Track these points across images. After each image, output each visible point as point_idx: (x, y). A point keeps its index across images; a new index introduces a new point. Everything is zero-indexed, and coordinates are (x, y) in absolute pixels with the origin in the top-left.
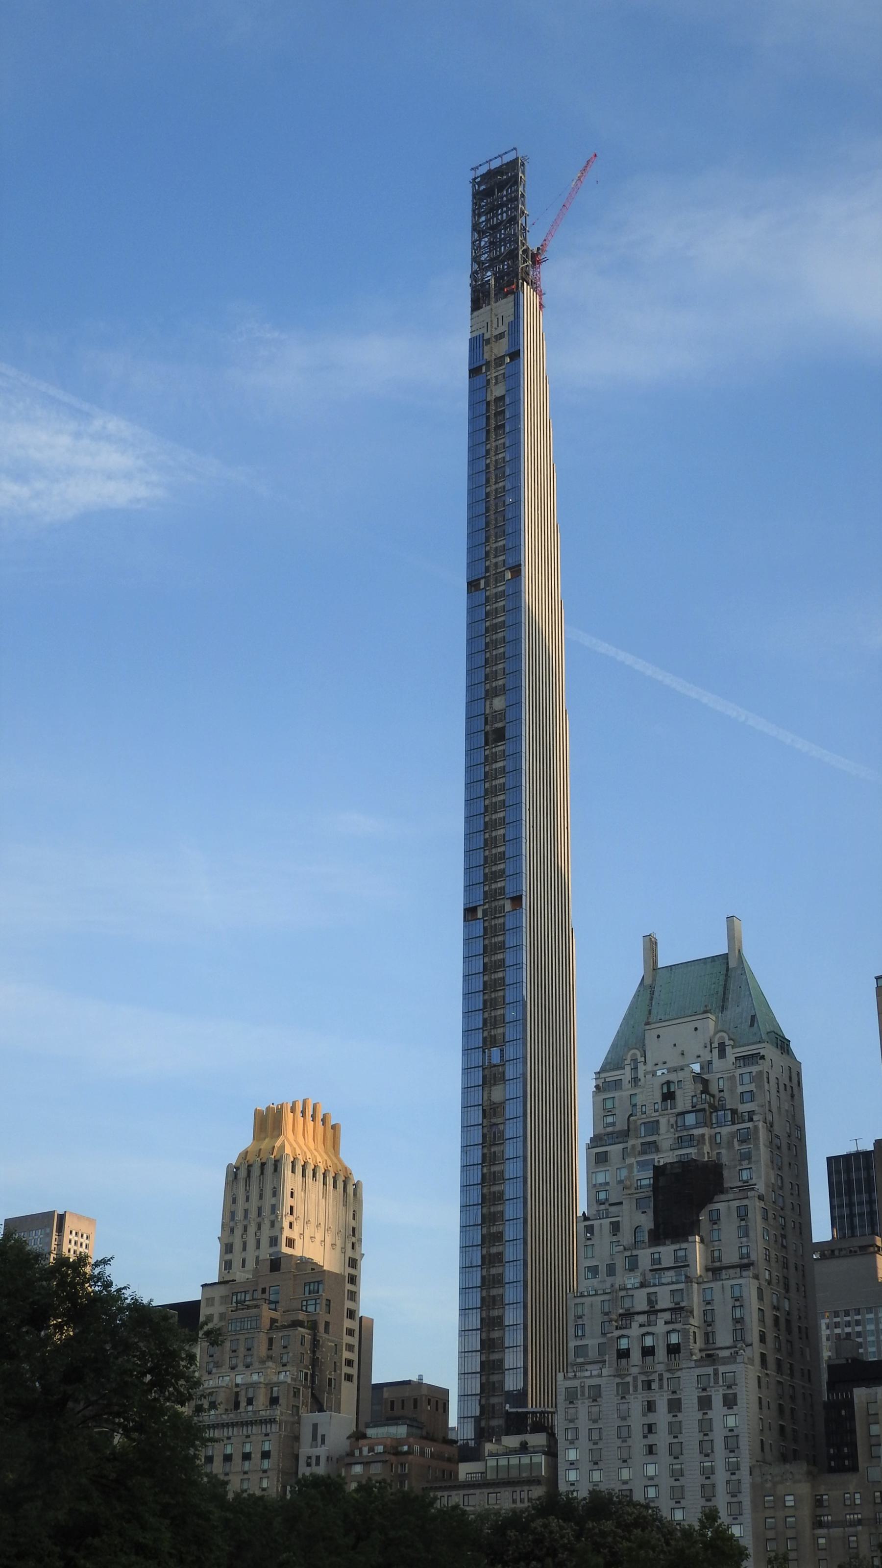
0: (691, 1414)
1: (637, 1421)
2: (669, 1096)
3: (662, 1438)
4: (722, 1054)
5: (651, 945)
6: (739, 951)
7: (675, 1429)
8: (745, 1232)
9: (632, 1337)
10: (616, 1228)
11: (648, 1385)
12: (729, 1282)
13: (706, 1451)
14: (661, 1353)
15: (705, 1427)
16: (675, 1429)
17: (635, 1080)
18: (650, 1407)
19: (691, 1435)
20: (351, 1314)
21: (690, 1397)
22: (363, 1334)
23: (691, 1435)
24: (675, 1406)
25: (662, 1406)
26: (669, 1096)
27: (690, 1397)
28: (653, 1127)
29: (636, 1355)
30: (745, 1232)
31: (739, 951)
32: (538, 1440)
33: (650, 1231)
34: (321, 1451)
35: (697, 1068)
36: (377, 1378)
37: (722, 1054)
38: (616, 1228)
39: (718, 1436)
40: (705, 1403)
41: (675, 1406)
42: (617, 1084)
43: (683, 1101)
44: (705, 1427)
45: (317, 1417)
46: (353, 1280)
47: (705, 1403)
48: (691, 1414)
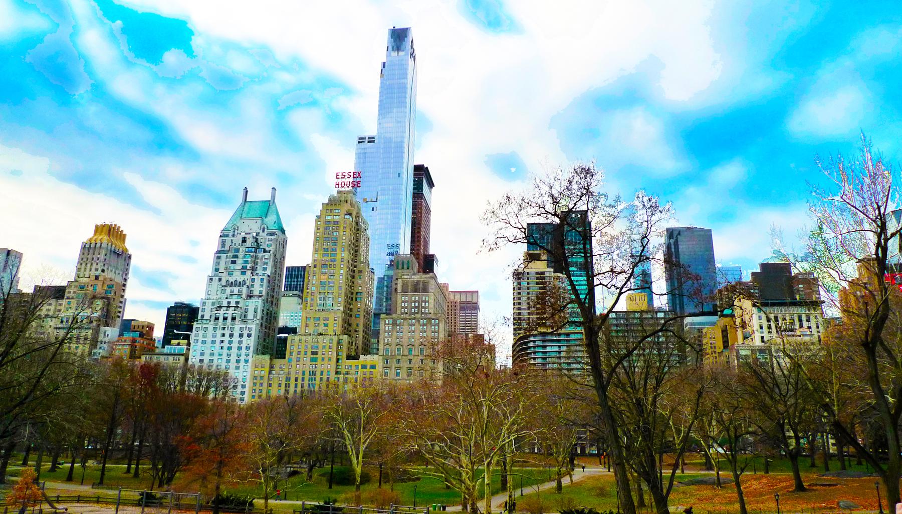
0: (236, 338)
1: (219, 338)
2: (244, 240)
3: (225, 345)
4: (263, 231)
5: (246, 192)
6: (157, 211)
7: (230, 342)
8: (262, 286)
9: (221, 313)
10: (220, 280)
11: (224, 329)
12: (254, 300)
13: (240, 348)
14: (229, 319)
15: (240, 342)
16: (230, 342)
17: (233, 235)
18: (223, 335)
19: (235, 345)
20: (122, 296)
21: (236, 333)
22: (123, 303)
23: (235, 345)
24: (231, 335)
25: (227, 335)
26: (244, 240)
27: (236, 333)
28: (237, 250)
29: (221, 319)
30: (262, 286)
31: (157, 211)
32: (186, 341)
33: (381, 280)
34: (106, 339)
35: (255, 235)
36: (125, 318)
37: (263, 231)
38: (220, 280)
39: (244, 346)
40: (241, 336)
41: (231, 335)
42: (227, 236)
43: (249, 243)
44: (240, 342)
45: (107, 328)
46: (124, 285)
47: (241, 336)
48: (236, 338)
